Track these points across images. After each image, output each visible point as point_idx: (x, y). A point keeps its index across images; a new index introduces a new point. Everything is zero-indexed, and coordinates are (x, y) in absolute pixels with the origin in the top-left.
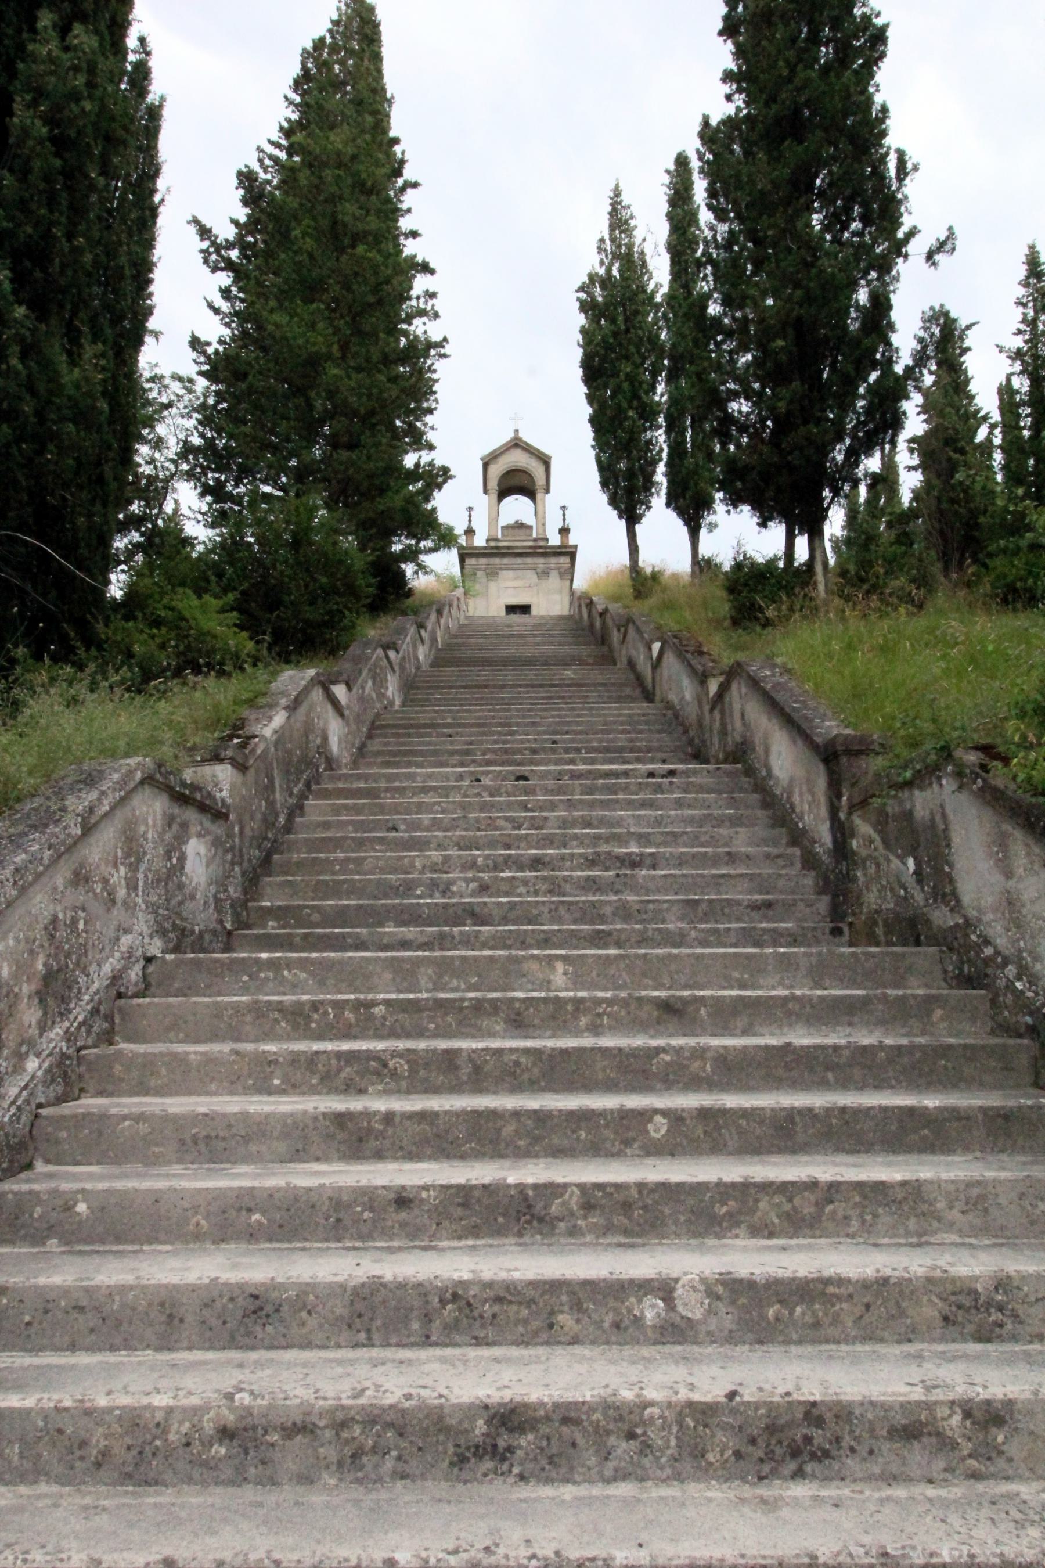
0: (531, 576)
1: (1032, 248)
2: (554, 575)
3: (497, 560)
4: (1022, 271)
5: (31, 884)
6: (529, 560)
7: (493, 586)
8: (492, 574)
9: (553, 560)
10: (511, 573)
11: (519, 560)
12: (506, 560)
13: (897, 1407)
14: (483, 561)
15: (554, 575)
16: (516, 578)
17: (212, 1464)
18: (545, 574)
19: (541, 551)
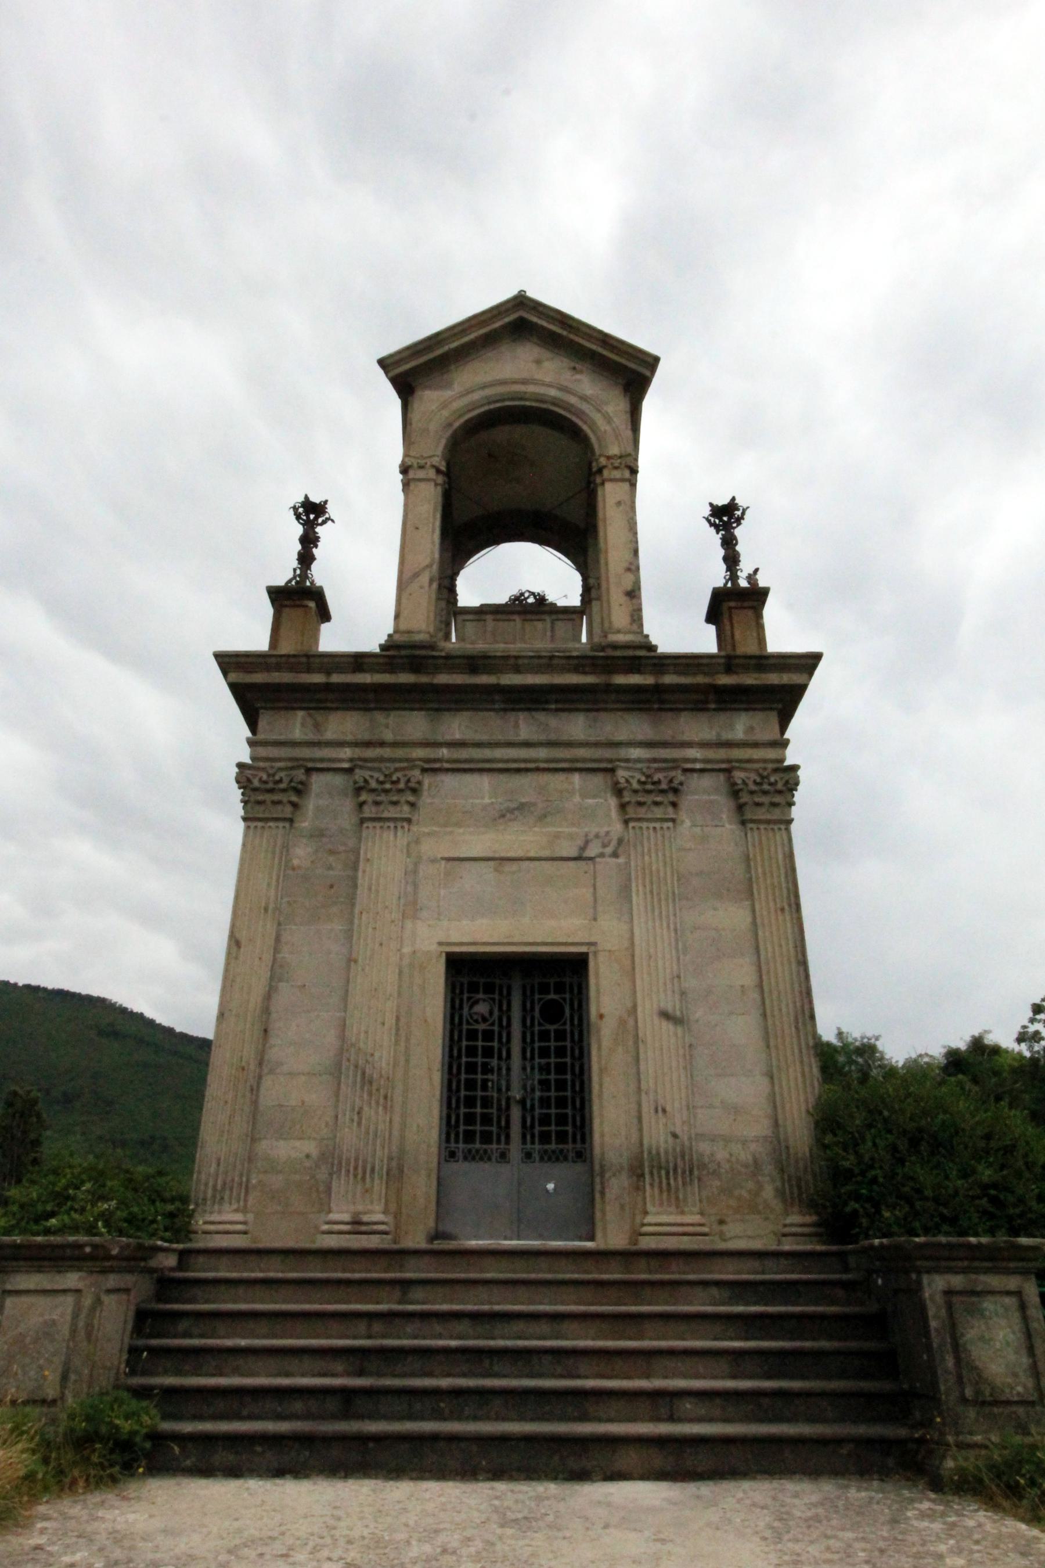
0: (587, 808)
1: (839, 1029)
2: (704, 792)
3: (414, 725)
4: (713, 530)
5: (415, 893)
6: (576, 726)
7: (385, 855)
8: (386, 793)
9: (695, 728)
10: (481, 790)
11: (525, 726)
12: (457, 726)
13: (946, 1489)
14: (343, 725)
15: (704, 792)
16: (510, 813)
17: (97, 1453)
18: (654, 794)
19: (625, 678)
